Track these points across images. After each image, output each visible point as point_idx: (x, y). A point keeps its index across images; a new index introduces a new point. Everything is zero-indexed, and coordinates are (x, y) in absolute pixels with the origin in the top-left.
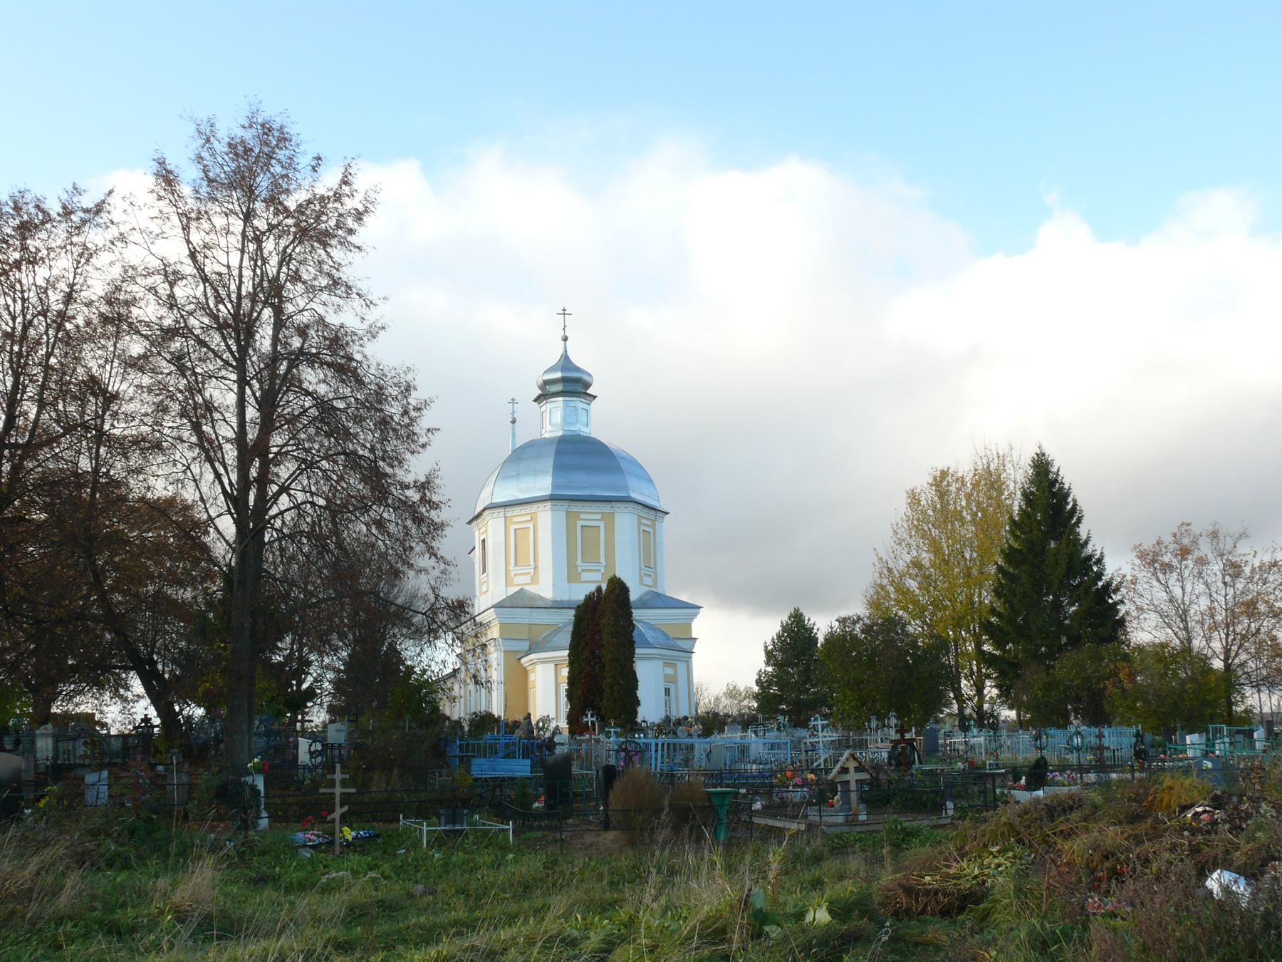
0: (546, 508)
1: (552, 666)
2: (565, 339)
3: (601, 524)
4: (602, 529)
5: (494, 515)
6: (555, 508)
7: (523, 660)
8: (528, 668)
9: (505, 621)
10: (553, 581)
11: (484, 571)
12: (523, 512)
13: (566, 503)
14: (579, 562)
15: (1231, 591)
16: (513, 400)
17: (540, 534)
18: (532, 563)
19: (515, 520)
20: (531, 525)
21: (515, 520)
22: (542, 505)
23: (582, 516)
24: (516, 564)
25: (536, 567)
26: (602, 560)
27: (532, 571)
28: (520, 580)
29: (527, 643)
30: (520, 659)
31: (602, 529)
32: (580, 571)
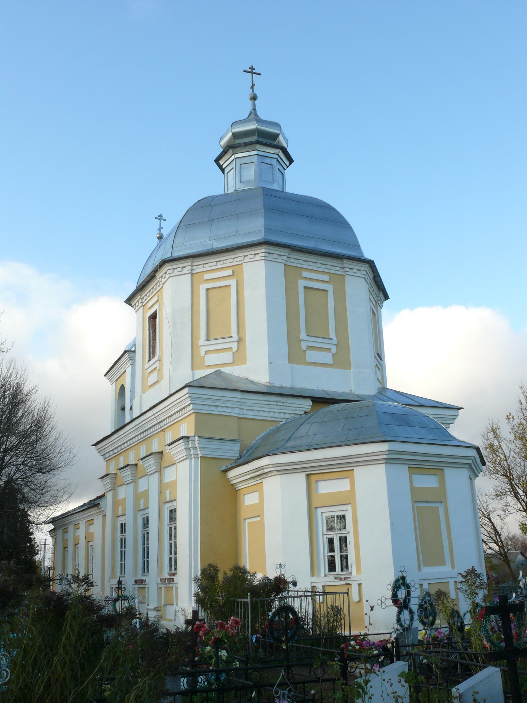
0: (257, 257)
1: (301, 478)
2: (254, 98)
3: (329, 287)
4: (331, 294)
5: (176, 272)
6: (270, 258)
7: (231, 474)
8: (240, 486)
9: (204, 410)
10: (269, 357)
11: (152, 353)
12: (220, 265)
13: (285, 252)
14: (303, 335)
15: (508, 508)
16: (161, 216)
17: (247, 293)
18: (234, 333)
19: (207, 276)
20: (232, 282)
21: (207, 276)
22: (250, 252)
23: (305, 274)
24: (208, 338)
25: (240, 340)
26: (332, 335)
27: (234, 346)
28: (213, 359)
29: (237, 447)
30: (225, 471)
31: (331, 294)
32: (304, 346)
